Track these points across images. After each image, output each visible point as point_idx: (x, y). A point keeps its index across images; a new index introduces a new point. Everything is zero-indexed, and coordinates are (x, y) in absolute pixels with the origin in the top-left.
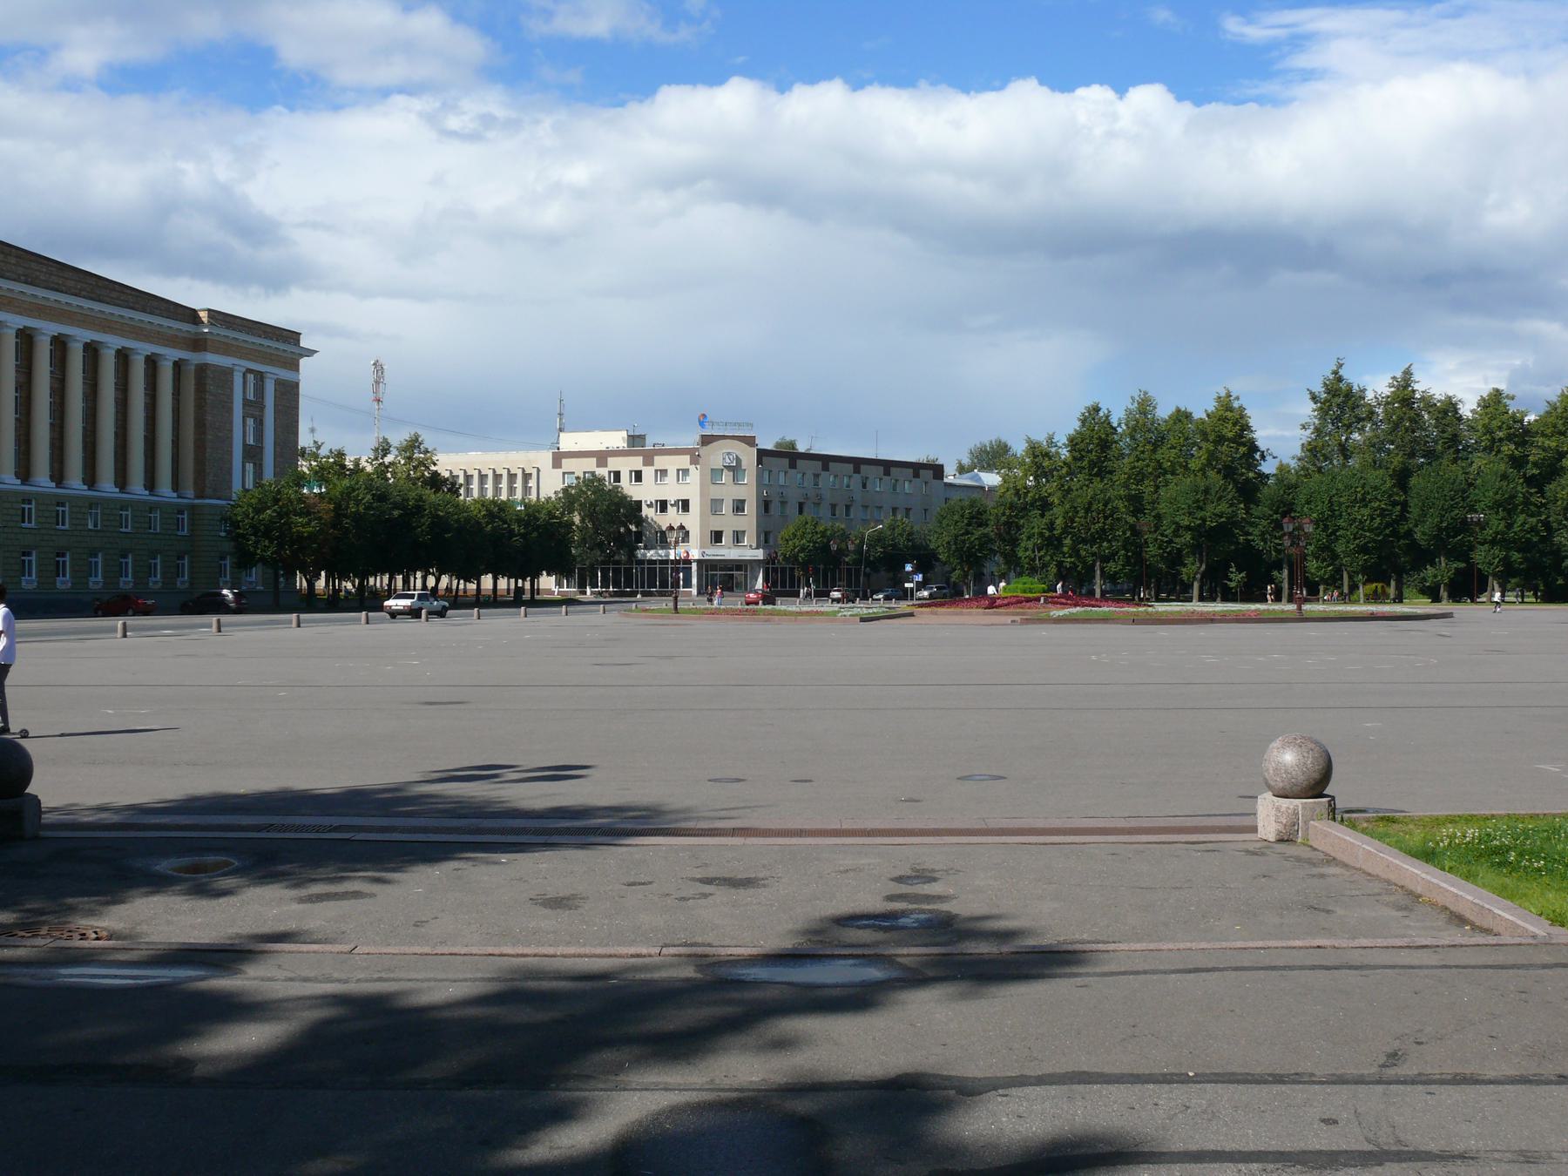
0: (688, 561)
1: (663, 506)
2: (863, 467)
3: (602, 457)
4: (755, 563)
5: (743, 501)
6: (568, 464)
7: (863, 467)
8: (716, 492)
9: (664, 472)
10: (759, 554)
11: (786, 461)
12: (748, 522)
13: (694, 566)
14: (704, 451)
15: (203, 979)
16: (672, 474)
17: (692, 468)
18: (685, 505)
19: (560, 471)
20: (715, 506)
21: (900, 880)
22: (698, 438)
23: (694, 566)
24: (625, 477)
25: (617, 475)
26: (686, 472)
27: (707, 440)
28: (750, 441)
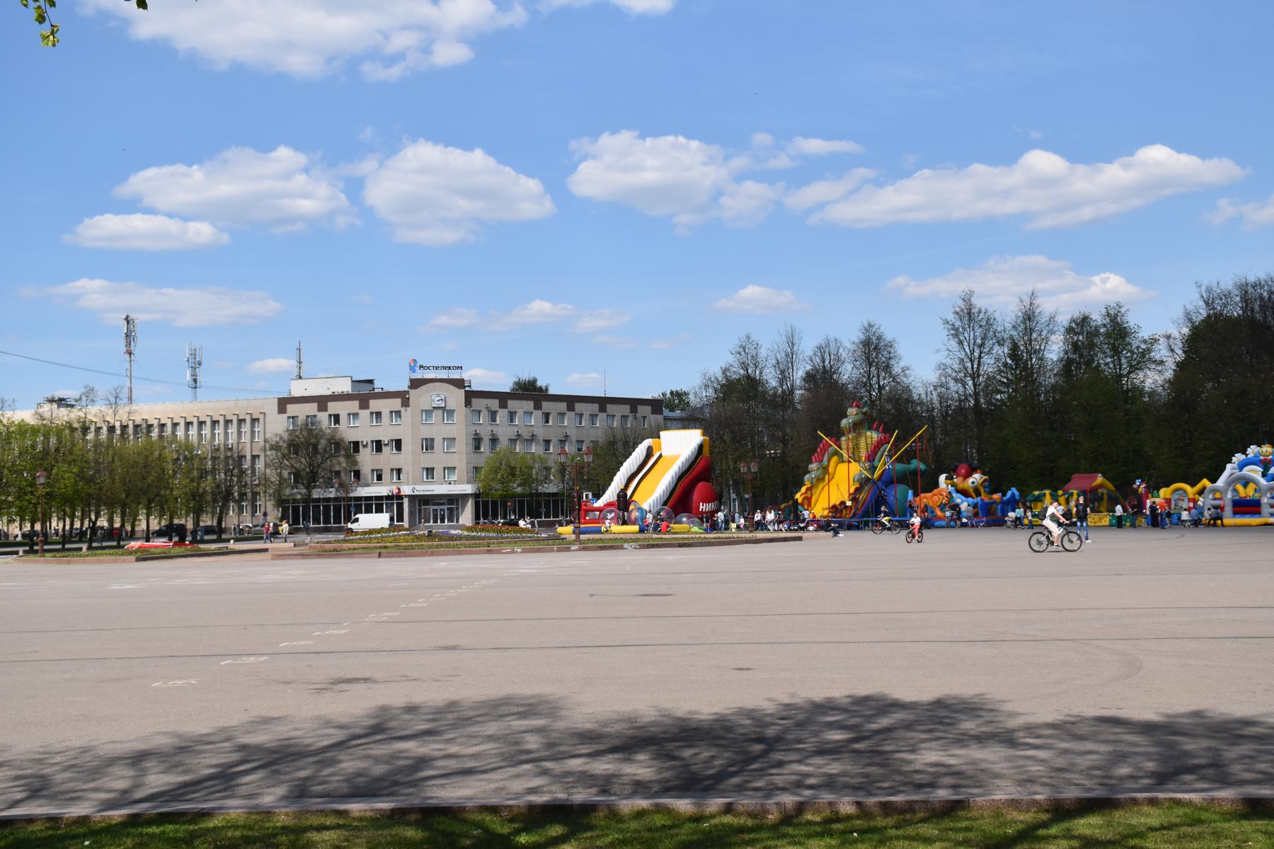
0: (399, 497)
1: (379, 446)
2: (609, 407)
3: (322, 402)
4: (464, 497)
5: (433, 440)
6: (292, 409)
7: (609, 407)
8: (426, 432)
9: (379, 414)
10: (468, 489)
11: (596, 406)
12: (460, 456)
13: (406, 501)
14: (413, 394)
15: (154, 808)
16: (385, 415)
17: (403, 410)
18: (398, 444)
19: (285, 416)
20: (429, 445)
21: (800, 539)
22: (407, 383)
23: (406, 501)
24: (343, 418)
25: (337, 418)
26: (356, 415)
27: (416, 384)
28: (459, 383)
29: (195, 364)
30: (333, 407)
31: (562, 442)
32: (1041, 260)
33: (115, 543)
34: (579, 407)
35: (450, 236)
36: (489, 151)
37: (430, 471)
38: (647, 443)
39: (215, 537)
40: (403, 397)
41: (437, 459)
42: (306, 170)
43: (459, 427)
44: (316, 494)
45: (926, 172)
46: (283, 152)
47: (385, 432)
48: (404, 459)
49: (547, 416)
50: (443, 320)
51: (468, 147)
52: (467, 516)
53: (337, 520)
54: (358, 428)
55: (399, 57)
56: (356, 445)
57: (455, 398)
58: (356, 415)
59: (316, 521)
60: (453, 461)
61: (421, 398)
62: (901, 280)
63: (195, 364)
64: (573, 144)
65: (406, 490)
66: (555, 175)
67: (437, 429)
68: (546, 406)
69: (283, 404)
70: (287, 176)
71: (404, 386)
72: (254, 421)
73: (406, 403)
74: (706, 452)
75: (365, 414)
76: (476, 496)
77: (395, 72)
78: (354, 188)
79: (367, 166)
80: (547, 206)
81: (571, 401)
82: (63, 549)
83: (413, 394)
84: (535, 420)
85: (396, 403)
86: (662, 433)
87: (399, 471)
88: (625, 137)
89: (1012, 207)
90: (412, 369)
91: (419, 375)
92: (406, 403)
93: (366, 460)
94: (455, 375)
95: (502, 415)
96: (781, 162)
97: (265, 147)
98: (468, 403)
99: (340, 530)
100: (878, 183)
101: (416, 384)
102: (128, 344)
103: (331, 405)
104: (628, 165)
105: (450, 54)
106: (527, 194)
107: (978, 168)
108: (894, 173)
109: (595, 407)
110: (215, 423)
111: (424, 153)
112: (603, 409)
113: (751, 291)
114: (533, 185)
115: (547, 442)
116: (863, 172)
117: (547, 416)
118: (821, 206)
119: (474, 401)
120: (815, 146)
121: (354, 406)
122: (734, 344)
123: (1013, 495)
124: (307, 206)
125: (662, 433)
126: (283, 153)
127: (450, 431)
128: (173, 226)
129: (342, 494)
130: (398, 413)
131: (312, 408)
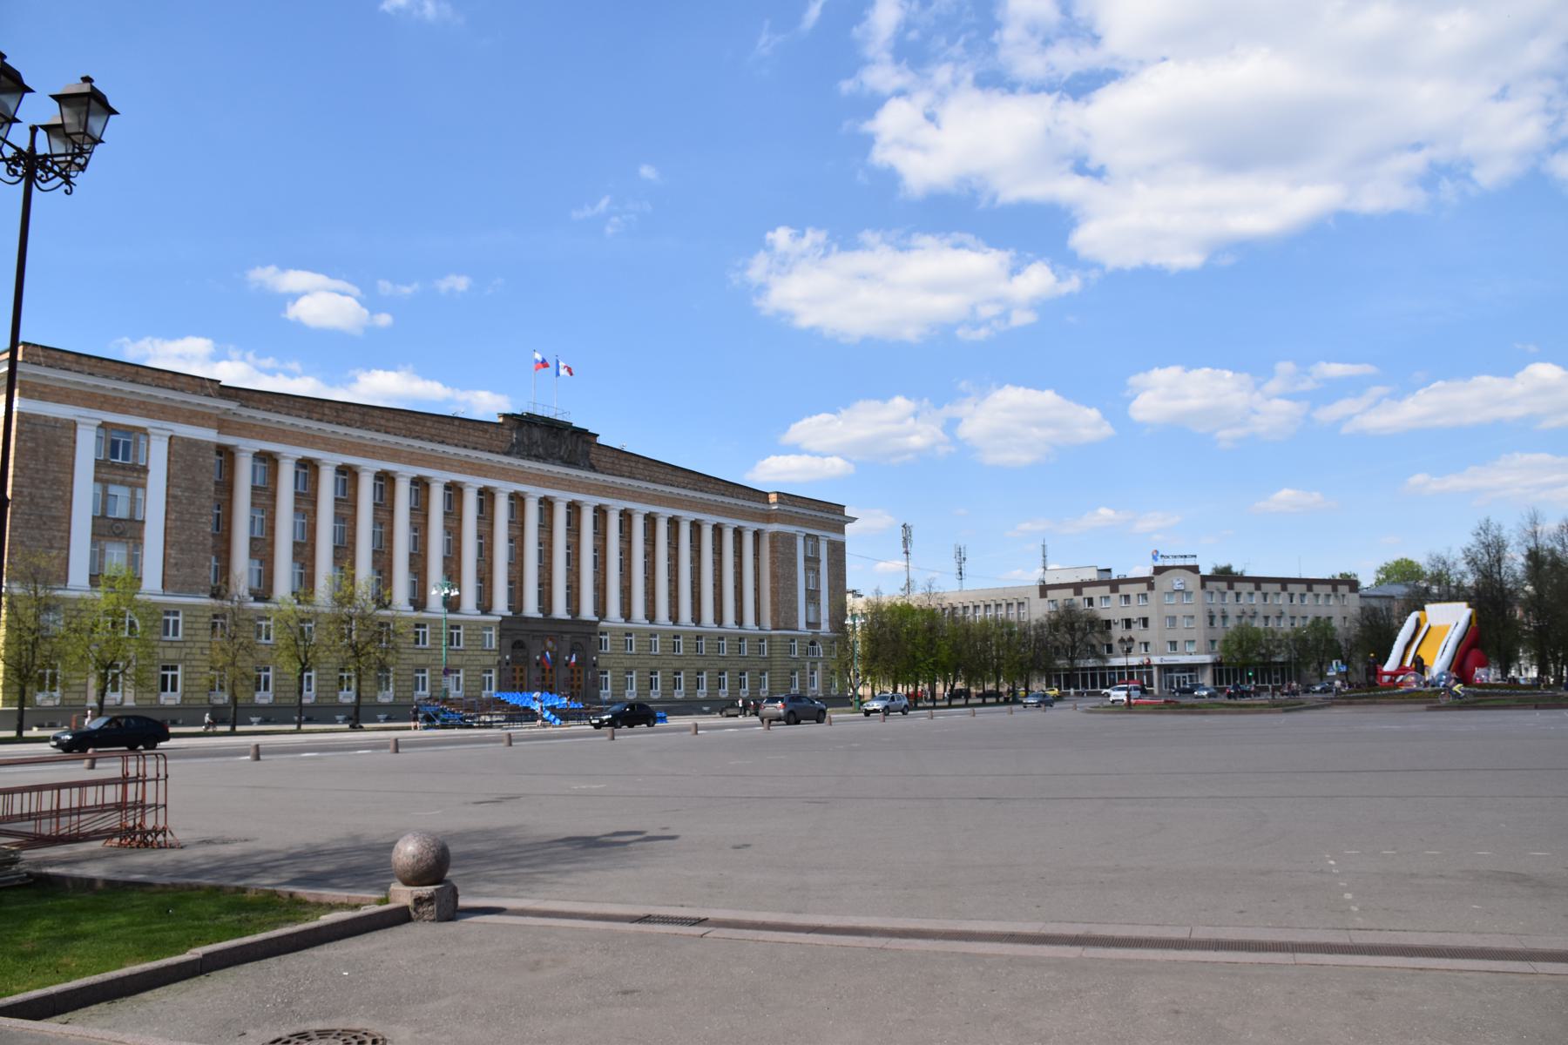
0: (1149, 666)
3: (1078, 587)
4: (1203, 666)
6: (1051, 594)
8: (1169, 611)
9: (1127, 597)
10: (1207, 659)
12: (1199, 631)
14: (1157, 579)
18: (1145, 622)
24: (1096, 601)
25: (1091, 601)
28: (1195, 569)
29: (961, 558)
30: (1087, 592)
31: (1279, 618)
32: (1545, 457)
33: (13, 734)
34: (1316, 588)
35: (1026, 458)
36: (1057, 392)
37: (1173, 644)
38: (1415, 615)
39: (227, 728)
40: (1149, 582)
41: (1178, 635)
42: (915, 415)
43: (1197, 604)
44: (1082, 663)
45: (1440, 383)
46: (899, 401)
47: (1134, 612)
48: (1149, 635)
49: (1291, 596)
50: (1026, 526)
51: (1040, 387)
52: (1207, 679)
53: (1094, 686)
54: (1110, 608)
55: (987, 322)
56: (1108, 623)
57: (1193, 582)
58: (1107, 598)
59: (1085, 686)
60: (1193, 635)
61: (1161, 582)
62: (1419, 478)
63: (961, 558)
64: (1133, 380)
65: (1156, 660)
66: (1114, 402)
67: (1179, 607)
68: (1238, 586)
69: (1044, 589)
70: (900, 421)
71: (1146, 571)
72: (1020, 604)
73: (1151, 587)
74: (1474, 623)
75: (1115, 596)
76: (1213, 664)
77: (983, 333)
78: (952, 424)
79: (965, 408)
80: (1107, 430)
81: (1258, 582)
82: (950, 706)
83: (1157, 579)
84: (1257, 599)
85: (1143, 587)
86: (1427, 607)
87: (1146, 644)
88: (1173, 372)
89: (1518, 411)
90: (1155, 558)
91: (1160, 563)
92: (1151, 587)
93: (1118, 632)
94: (1190, 562)
95: (1231, 594)
96: (1308, 385)
97: (885, 396)
98: (1203, 586)
99: (1099, 694)
100: (1398, 397)
101: (1159, 570)
102: (905, 545)
103: (1085, 590)
104: (1169, 392)
105: (1021, 318)
106: (1088, 422)
107: (1485, 379)
108: (1405, 389)
109: (1303, 587)
110: (1009, 605)
111: (1013, 395)
112: (1310, 589)
113: (1285, 494)
114: (1094, 414)
115: (1267, 618)
116: (1378, 390)
117: (1265, 595)
118: (1350, 417)
119: (1049, 593)
120: (1336, 370)
121: (1106, 590)
122: (1474, 525)
123: (93, 718)
124: (916, 441)
125: (1427, 607)
126: (900, 403)
127: (1190, 610)
128: (815, 462)
129: (1100, 664)
130: (1145, 596)
131: (1069, 593)
